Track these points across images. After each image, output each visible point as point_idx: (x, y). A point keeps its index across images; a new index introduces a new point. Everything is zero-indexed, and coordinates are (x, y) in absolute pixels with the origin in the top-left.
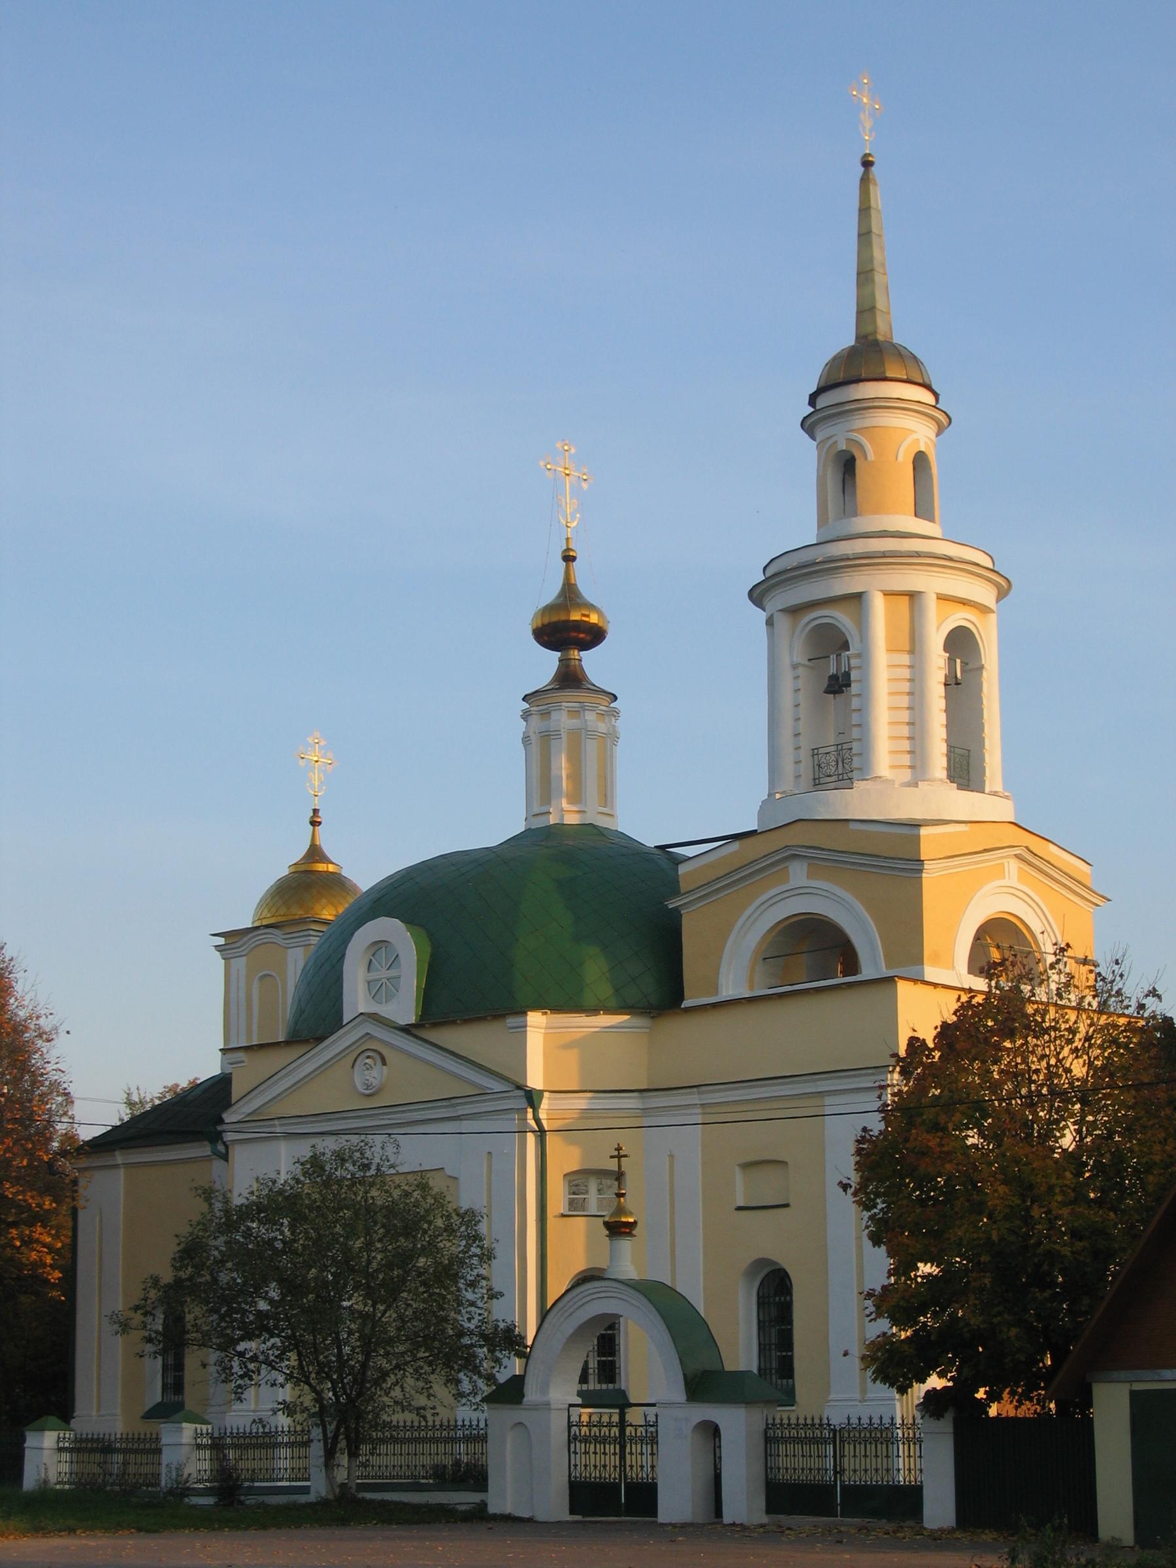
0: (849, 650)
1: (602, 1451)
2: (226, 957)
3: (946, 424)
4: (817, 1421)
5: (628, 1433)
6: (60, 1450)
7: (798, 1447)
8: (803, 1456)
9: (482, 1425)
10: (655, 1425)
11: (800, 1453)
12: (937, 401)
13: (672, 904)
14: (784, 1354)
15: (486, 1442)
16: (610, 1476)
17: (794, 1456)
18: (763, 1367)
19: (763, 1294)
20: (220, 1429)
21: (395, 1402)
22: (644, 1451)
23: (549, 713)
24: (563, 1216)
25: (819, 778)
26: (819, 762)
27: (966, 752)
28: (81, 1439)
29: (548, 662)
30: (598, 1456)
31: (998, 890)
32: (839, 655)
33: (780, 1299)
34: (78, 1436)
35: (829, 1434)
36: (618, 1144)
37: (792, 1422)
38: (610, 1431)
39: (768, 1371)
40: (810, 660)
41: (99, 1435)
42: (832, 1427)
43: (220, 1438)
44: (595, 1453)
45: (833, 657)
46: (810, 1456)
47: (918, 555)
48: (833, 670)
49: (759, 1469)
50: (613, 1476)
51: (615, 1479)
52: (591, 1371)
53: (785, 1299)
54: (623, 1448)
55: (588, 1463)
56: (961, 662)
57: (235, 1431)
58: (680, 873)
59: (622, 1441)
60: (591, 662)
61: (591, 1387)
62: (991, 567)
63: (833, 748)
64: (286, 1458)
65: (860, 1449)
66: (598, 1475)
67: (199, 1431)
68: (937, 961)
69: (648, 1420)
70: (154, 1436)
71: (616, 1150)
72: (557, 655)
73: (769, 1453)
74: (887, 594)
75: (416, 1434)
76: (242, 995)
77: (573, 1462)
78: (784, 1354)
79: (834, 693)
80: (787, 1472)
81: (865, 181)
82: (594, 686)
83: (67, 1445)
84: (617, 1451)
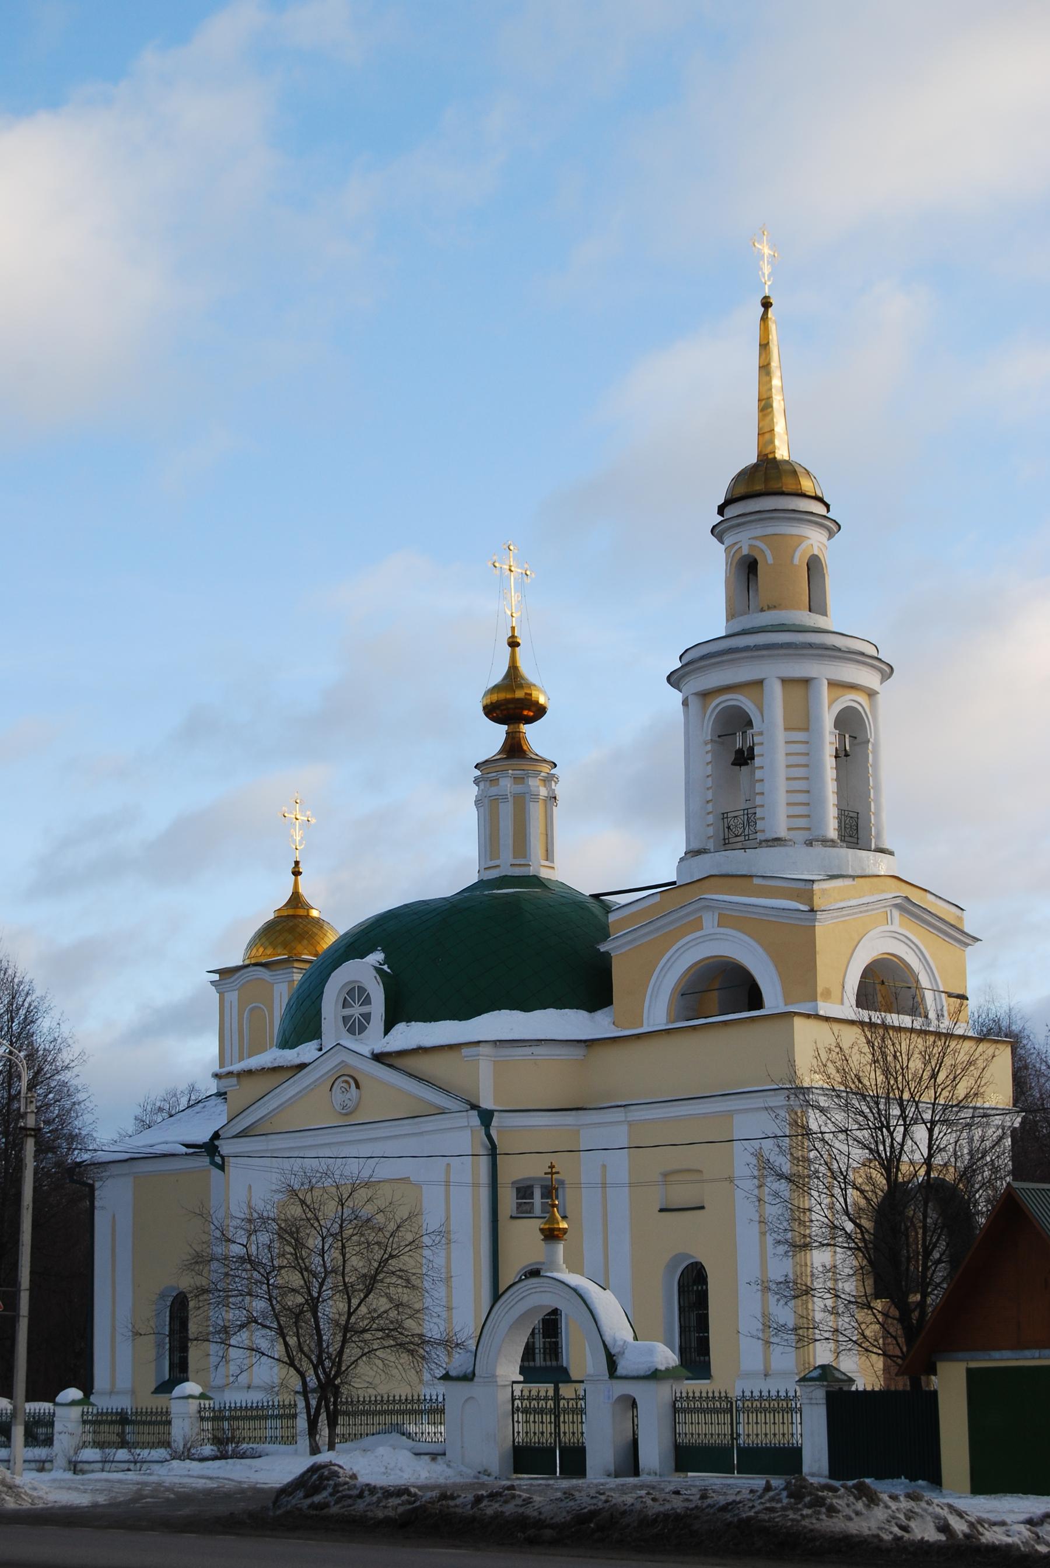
0: (753, 729)
1: (540, 1420)
2: (220, 991)
3: (836, 530)
4: (717, 1394)
5: (561, 1405)
6: (84, 1422)
7: (701, 1416)
8: (705, 1423)
9: (440, 1399)
10: (584, 1398)
11: (704, 1421)
12: (828, 511)
13: (603, 948)
14: (701, 1335)
15: (444, 1413)
16: (547, 1441)
17: (698, 1423)
18: (683, 1346)
19: (683, 1284)
20: (220, 1404)
21: (889, 1160)
22: (575, 1420)
23: (498, 779)
24: (511, 1217)
25: (729, 838)
26: (728, 824)
27: (855, 815)
28: (102, 1413)
29: (499, 733)
30: (537, 1425)
31: (882, 935)
32: (744, 733)
33: (698, 1288)
34: (100, 1411)
35: (727, 1405)
36: (551, 1163)
37: (696, 1395)
38: (546, 1403)
39: (688, 1350)
40: (719, 736)
41: (122, 1409)
42: (729, 1399)
43: (220, 1411)
44: (534, 1422)
45: (739, 735)
46: (712, 1424)
47: (811, 646)
48: (739, 745)
49: (668, 1435)
50: (549, 1441)
51: (551, 1443)
52: (537, 1351)
53: (702, 1288)
54: (557, 1417)
55: (528, 1430)
56: (850, 736)
57: (233, 1405)
58: (609, 921)
59: (556, 1412)
60: (533, 734)
61: (538, 1365)
62: (876, 655)
63: (741, 812)
64: (276, 1428)
65: (753, 1417)
66: (537, 1440)
67: (202, 1406)
68: (827, 994)
69: (578, 1393)
70: (164, 1410)
71: (549, 1167)
72: (504, 728)
73: (677, 1421)
74: (785, 681)
75: (385, 1407)
76: (235, 1026)
77: (516, 1430)
78: (701, 1335)
79: (740, 765)
80: (712, 1437)
81: (764, 318)
82: (537, 755)
83: (90, 1418)
84: (553, 1420)
